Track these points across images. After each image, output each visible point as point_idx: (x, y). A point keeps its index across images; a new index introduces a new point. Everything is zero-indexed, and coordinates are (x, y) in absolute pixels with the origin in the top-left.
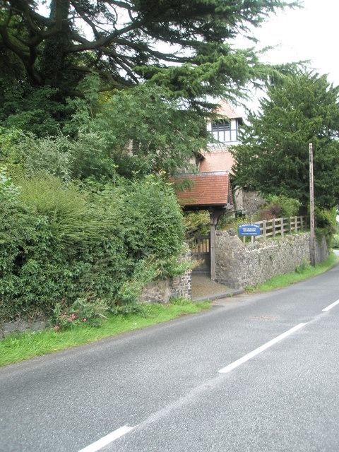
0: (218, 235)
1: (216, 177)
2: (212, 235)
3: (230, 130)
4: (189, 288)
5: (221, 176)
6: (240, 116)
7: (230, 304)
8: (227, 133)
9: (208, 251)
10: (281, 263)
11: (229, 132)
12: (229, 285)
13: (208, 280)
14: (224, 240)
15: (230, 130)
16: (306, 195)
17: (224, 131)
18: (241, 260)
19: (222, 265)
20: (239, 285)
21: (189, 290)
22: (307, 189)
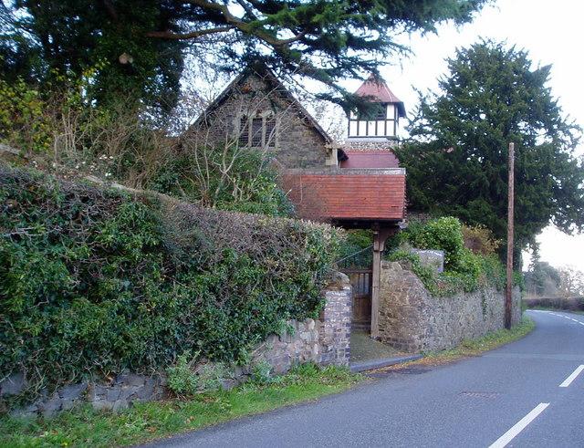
0: (384, 267)
1: (385, 177)
2: (376, 267)
3: (386, 120)
4: (347, 346)
5: (393, 177)
6: (402, 100)
7: (258, 407)
8: (381, 124)
9: (367, 291)
10: (471, 318)
11: (383, 122)
12: (398, 347)
13: (365, 337)
14: (388, 274)
15: (386, 120)
16: (500, 221)
17: (376, 121)
18: (420, 308)
19: (389, 315)
20: (414, 347)
21: (347, 350)
22: (504, 211)
